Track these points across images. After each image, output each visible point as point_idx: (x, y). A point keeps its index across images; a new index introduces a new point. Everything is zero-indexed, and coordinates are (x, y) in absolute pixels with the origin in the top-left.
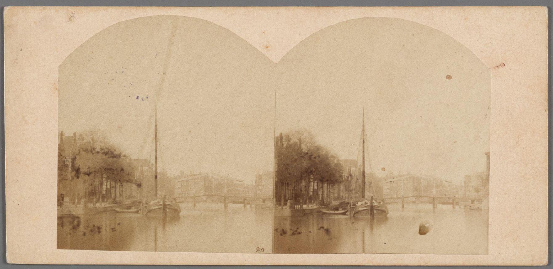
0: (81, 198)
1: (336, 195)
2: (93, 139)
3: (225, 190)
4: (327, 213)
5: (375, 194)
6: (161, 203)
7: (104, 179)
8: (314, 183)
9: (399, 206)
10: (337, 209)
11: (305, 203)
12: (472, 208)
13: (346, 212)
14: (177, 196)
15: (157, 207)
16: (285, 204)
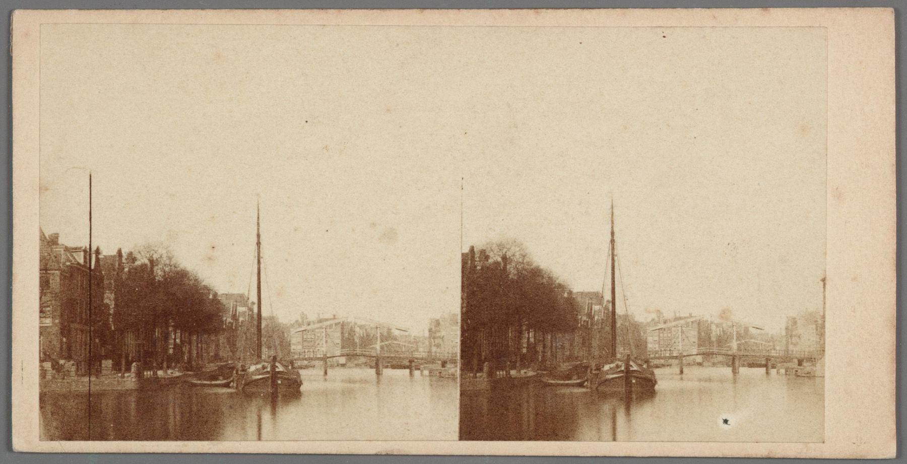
0: (132, 362)
1: (568, 353)
2: (151, 261)
3: (734, 345)
4: (551, 385)
5: (634, 351)
6: (623, 368)
7: (171, 329)
8: (175, 334)
9: (318, 372)
10: (215, 378)
11: (513, 368)
12: (444, 373)
13: (584, 382)
14: (296, 357)
15: (261, 377)
16: (128, 370)
